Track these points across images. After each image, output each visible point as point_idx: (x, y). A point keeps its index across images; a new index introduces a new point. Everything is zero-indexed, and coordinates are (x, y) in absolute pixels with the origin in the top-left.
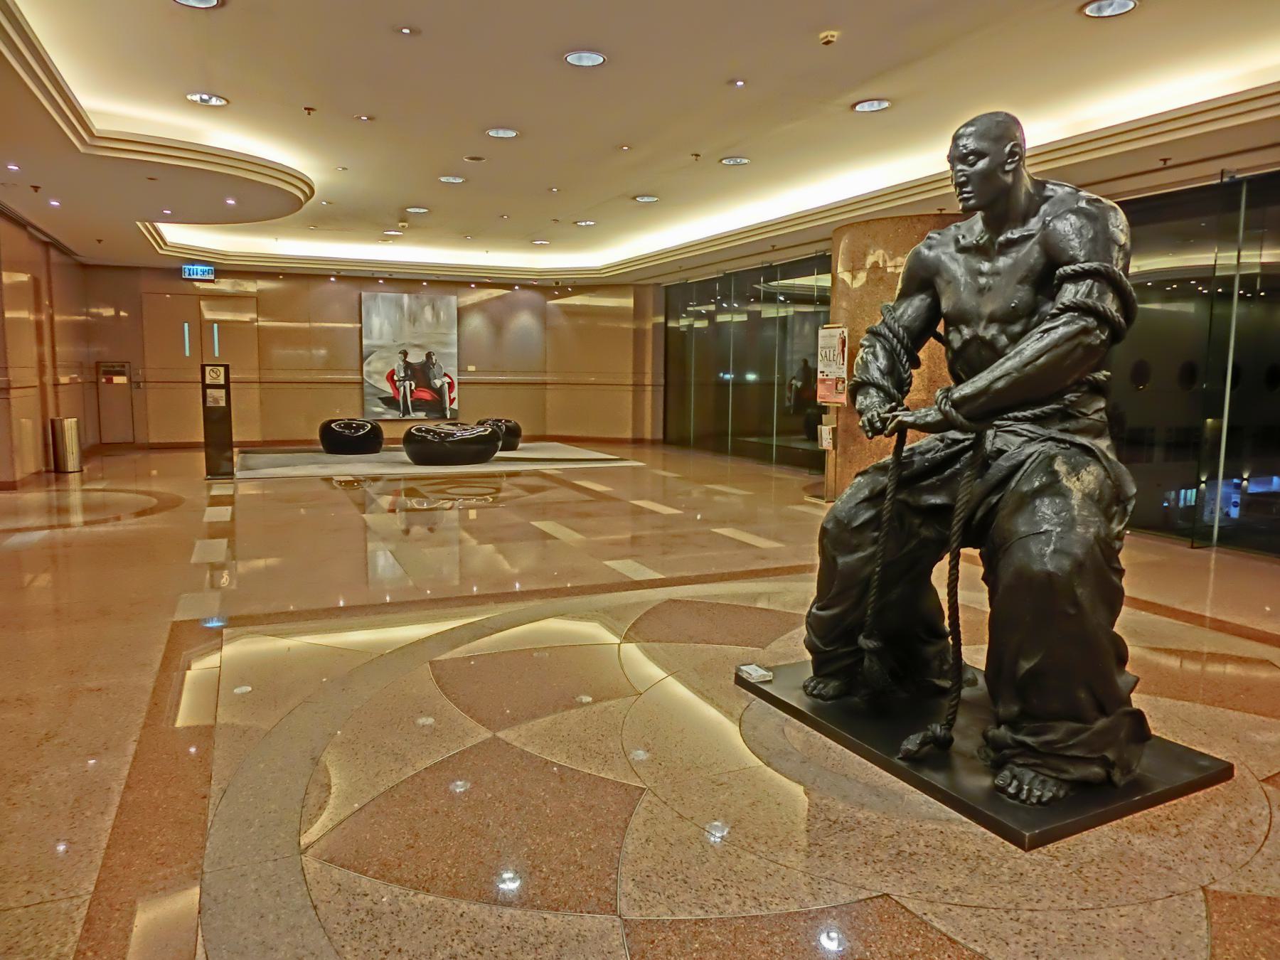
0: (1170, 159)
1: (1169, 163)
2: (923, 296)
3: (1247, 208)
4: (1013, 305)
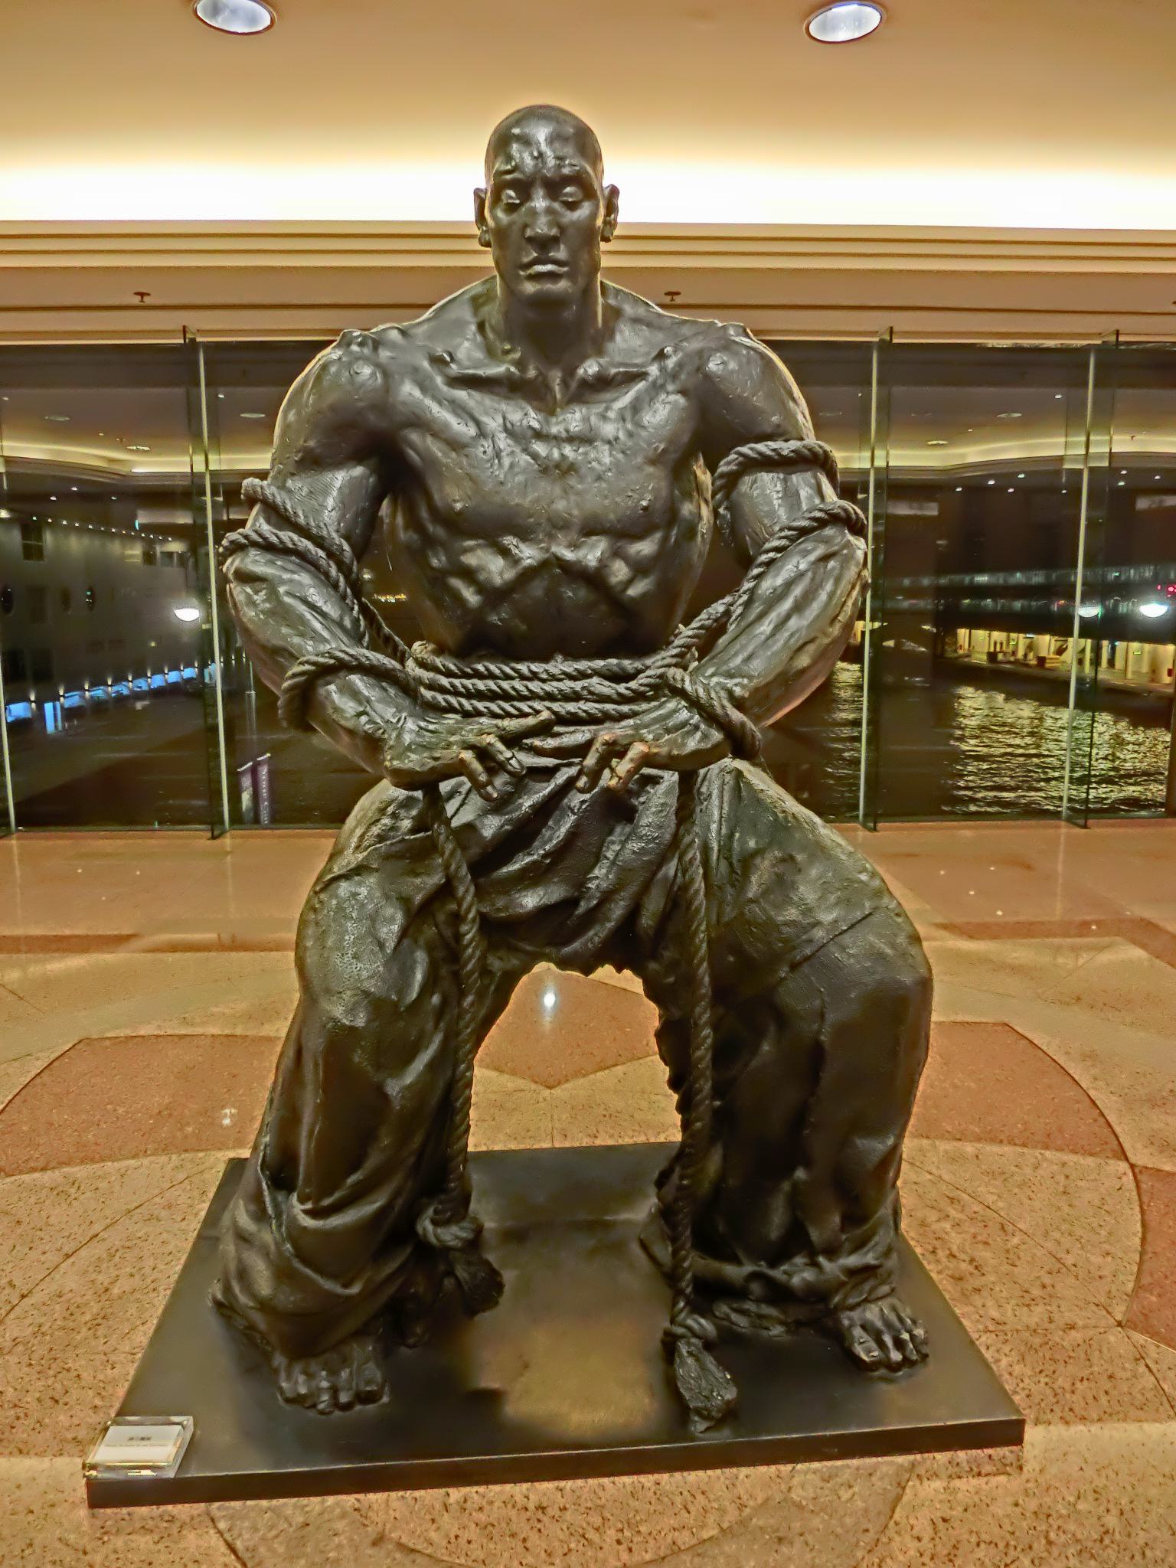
0: (678, 293)
1: (148, 300)
2: (358, 471)
3: (1095, 386)
4: (644, 503)
